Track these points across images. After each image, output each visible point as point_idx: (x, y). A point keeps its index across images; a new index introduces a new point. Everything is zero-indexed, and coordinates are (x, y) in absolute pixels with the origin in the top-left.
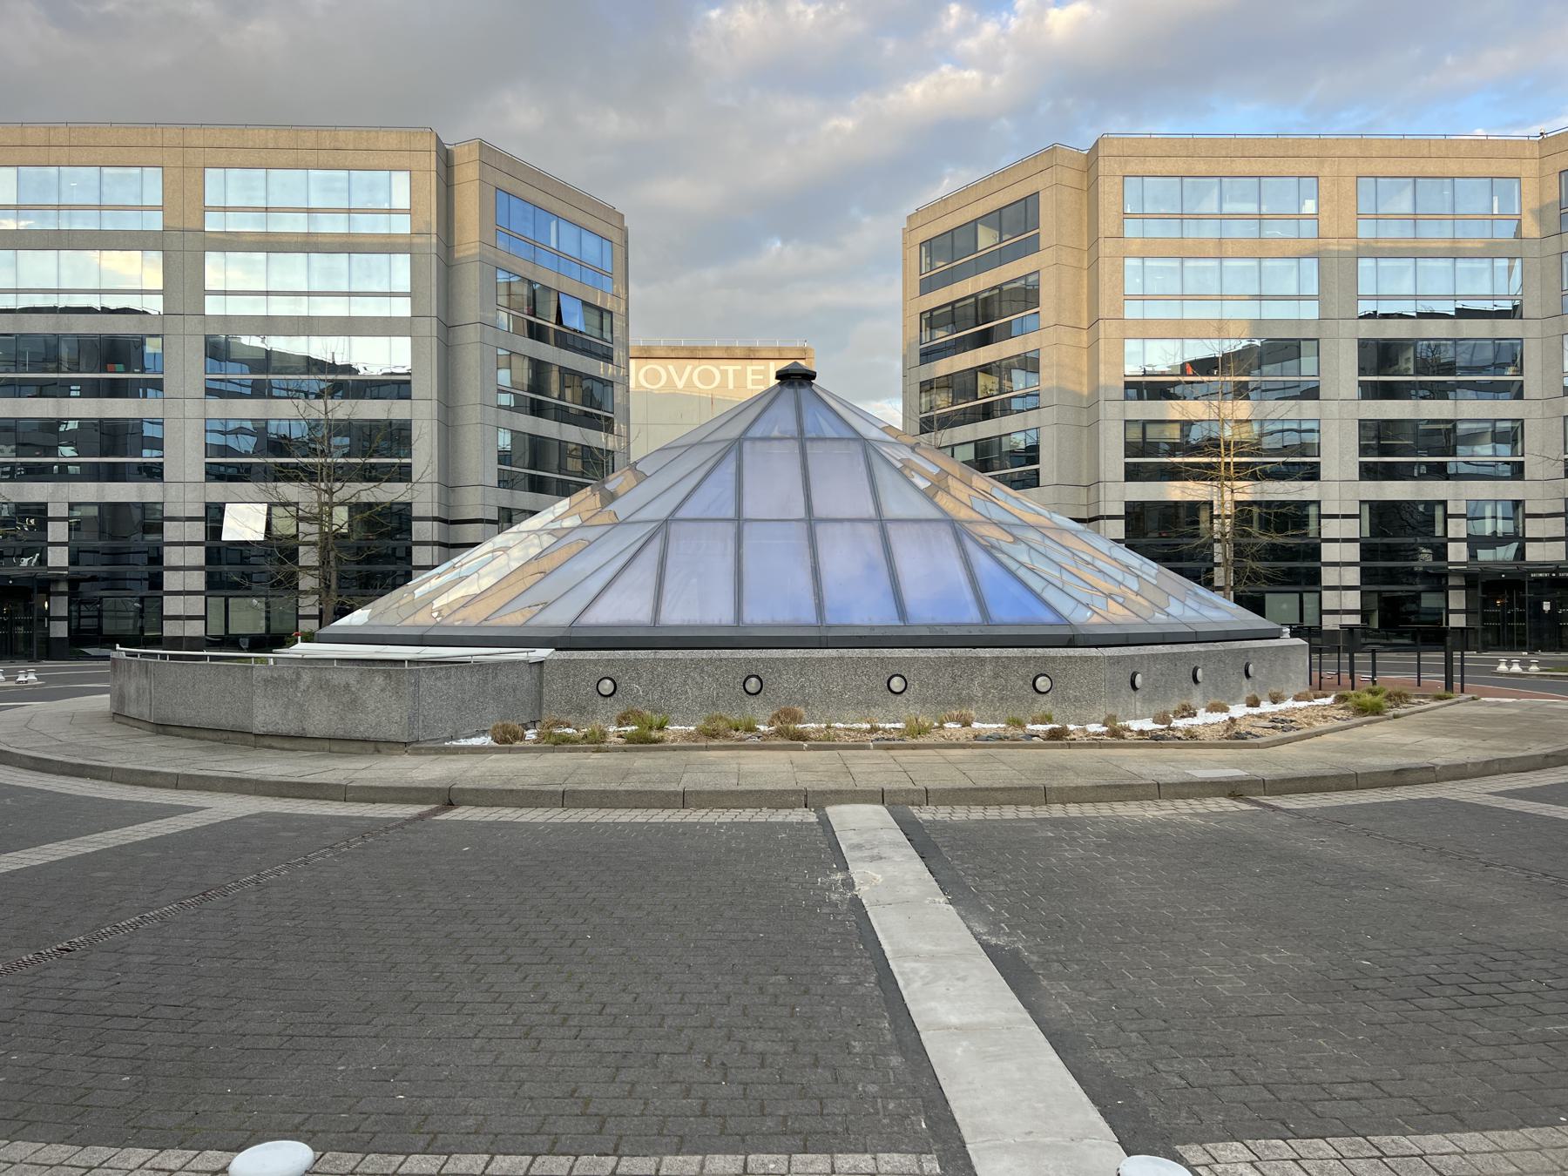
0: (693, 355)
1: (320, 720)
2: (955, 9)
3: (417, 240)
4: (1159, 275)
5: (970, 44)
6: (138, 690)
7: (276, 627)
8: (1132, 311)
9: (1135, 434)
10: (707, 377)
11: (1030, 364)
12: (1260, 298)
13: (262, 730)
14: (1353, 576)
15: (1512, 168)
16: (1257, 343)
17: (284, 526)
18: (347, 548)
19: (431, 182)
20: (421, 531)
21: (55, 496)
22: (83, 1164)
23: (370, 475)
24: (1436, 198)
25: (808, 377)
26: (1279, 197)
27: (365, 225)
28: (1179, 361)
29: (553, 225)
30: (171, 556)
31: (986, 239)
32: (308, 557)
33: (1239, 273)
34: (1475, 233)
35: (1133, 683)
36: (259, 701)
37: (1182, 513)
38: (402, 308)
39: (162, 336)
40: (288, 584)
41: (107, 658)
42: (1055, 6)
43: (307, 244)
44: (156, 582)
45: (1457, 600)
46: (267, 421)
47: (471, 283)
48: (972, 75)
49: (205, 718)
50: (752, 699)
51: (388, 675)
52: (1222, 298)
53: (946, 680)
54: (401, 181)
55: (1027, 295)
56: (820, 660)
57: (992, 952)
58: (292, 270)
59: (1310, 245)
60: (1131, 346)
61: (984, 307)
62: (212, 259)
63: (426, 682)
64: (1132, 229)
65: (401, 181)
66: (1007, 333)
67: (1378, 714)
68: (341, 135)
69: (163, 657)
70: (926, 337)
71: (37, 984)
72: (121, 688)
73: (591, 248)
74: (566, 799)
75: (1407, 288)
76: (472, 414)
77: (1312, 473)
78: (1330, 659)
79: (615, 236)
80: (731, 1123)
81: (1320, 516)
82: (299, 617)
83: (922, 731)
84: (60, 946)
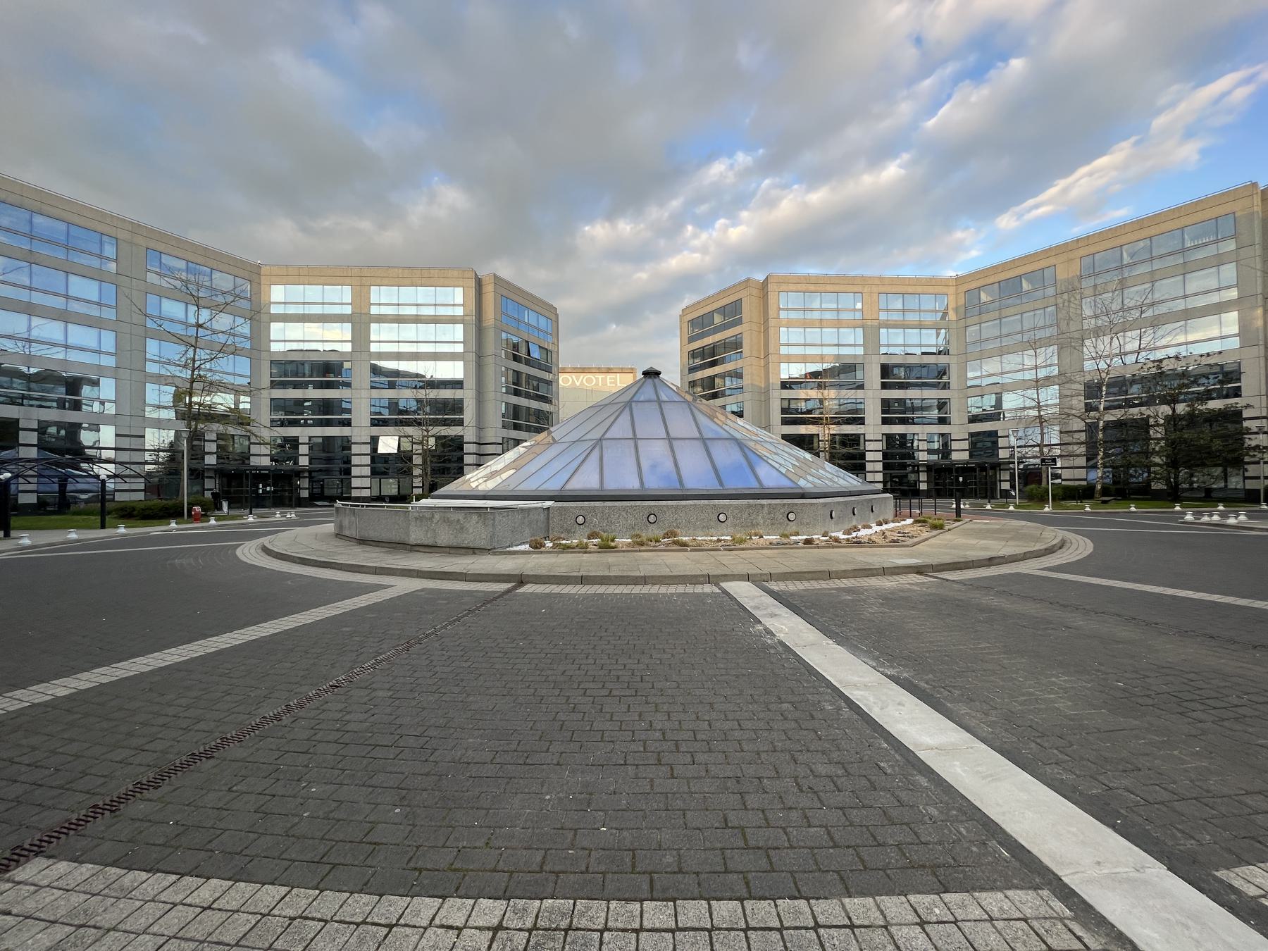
0: (583, 370)
1: (444, 538)
2: (690, 228)
3: (466, 318)
4: (795, 335)
5: (696, 243)
6: (349, 523)
7: (403, 492)
8: (783, 350)
9: (786, 404)
10: (589, 380)
11: (738, 375)
12: (838, 345)
13: (415, 543)
14: (879, 467)
15: (945, 290)
16: (837, 365)
17: (407, 446)
18: (433, 456)
19: (472, 292)
20: (468, 448)
21: (302, 433)
22: (383, 921)
23: (445, 423)
24: (912, 303)
25: (658, 373)
26: (846, 301)
27: (442, 311)
28: (803, 373)
29: (526, 312)
30: (355, 460)
31: (718, 319)
32: (417, 460)
33: (829, 334)
34: (929, 318)
35: (831, 515)
36: (412, 528)
37: (807, 439)
38: (459, 348)
39: (351, 361)
40: (408, 472)
41: (333, 506)
42: (732, 227)
43: (417, 320)
44: (348, 472)
45: (923, 477)
46: (398, 399)
47: (490, 336)
48: (697, 255)
49: (385, 536)
50: (652, 525)
51: (480, 515)
52: (822, 345)
53: (745, 516)
54: (459, 291)
55: (736, 345)
56: (685, 506)
57: (895, 679)
58: (409, 331)
59: (859, 322)
60: (783, 366)
61: (713, 350)
62: (374, 326)
63: (498, 518)
64: (783, 315)
65: (459, 291)
66: (723, 361)
67: (942, 529)
68: (432, 271)
69: (363, 506)
70: (691, 362)
71: (321, 716)
72: (341, 521)
73: (543, 322)
74: (584, 580)
75: (900, 341)
76: (490, 395)
77: (861, 421)
78: (905, 502)
79: (553, 317)
80: (689, 759)
81: (865, 441)
82: (413, 487)
83: (742, 541)
84: (331, 683)
